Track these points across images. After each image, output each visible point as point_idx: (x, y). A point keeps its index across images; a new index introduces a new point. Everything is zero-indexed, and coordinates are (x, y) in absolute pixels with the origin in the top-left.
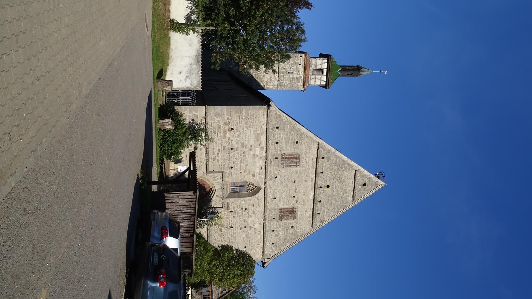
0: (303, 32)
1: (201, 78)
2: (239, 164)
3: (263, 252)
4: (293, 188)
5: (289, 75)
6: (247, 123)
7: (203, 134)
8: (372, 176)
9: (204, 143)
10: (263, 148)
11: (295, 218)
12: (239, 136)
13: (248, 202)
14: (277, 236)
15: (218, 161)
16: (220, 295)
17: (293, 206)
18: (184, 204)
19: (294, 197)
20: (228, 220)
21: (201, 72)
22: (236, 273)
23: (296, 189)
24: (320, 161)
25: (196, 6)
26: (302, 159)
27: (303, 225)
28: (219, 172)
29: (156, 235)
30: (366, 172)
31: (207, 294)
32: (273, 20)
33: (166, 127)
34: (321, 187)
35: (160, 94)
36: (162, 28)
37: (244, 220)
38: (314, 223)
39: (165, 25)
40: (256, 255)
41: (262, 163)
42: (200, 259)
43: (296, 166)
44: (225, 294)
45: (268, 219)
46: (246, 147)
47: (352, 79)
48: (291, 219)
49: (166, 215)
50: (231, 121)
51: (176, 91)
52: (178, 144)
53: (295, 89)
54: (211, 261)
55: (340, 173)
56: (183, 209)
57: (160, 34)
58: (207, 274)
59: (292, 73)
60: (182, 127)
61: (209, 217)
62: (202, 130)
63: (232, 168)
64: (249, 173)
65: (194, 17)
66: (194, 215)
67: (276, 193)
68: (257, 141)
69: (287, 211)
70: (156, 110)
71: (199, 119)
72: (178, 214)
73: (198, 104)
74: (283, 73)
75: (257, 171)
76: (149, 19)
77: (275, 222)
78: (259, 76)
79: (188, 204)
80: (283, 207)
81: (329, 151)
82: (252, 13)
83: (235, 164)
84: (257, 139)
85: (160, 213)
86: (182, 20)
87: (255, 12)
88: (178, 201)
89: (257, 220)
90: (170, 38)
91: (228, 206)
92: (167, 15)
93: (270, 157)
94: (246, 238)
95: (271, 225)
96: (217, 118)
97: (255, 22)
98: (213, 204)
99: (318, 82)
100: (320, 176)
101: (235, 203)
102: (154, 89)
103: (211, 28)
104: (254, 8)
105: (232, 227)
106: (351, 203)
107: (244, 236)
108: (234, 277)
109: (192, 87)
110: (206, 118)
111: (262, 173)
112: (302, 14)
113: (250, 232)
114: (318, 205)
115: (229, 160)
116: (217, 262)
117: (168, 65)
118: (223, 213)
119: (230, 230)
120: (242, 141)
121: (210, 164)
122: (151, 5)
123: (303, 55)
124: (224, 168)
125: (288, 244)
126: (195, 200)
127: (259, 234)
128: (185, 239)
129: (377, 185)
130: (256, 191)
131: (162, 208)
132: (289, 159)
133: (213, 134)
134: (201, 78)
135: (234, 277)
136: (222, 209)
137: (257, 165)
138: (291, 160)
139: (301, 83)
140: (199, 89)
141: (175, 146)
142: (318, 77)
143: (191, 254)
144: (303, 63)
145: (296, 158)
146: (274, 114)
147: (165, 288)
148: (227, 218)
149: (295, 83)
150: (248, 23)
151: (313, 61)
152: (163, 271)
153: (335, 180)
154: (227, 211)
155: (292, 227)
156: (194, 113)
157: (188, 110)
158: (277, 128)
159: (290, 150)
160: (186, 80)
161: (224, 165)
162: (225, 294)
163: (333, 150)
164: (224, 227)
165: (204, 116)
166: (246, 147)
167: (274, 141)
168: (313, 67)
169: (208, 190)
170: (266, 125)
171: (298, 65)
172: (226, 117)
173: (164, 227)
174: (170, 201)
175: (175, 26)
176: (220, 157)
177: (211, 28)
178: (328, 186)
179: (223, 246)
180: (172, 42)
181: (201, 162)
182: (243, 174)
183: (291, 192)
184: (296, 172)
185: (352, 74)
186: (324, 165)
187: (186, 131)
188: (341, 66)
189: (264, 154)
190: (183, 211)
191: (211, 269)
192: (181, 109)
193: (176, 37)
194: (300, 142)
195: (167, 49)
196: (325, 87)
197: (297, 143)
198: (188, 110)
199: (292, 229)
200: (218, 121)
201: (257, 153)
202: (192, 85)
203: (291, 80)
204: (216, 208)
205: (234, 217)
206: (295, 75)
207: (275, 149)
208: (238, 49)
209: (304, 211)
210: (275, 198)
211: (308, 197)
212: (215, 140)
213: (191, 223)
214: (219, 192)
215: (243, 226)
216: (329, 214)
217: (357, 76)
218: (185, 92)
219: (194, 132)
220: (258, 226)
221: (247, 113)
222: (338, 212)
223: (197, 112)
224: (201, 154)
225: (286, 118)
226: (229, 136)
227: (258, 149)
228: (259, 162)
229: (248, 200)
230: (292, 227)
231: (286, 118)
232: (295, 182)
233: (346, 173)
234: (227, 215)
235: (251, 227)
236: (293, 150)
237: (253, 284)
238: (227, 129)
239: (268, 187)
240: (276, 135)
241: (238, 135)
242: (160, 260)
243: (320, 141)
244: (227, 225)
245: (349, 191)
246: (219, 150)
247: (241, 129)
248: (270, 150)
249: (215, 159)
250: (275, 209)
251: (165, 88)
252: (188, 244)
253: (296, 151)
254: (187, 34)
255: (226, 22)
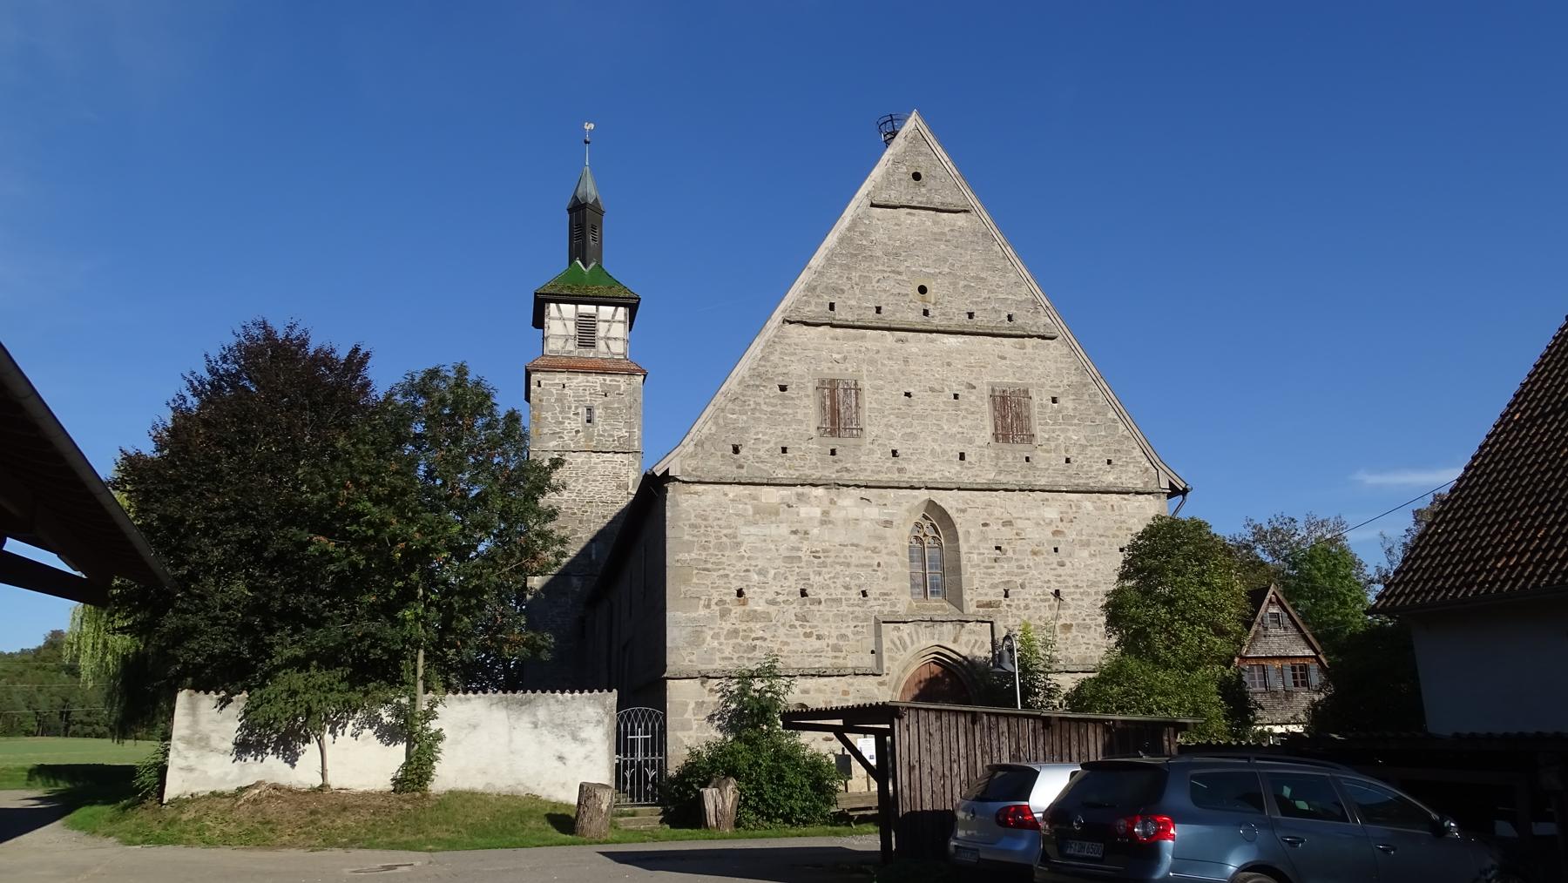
0: (433, 374)
1: (577, 694)
2: (853, 570)
3: (1138, 493)
4: (931, 403)
5: (596, 420)
6: (721, 547)
7: (757, 684)
8: (888, 155)
9: (785, 681)
10: (800, 496)
11: (1026, 392)
12: (762, 572)
13: (973, 541)
14: (1084, 447)
15: (843, 636)
16: (1292, 631)
17: (987, 398)
18: (937, 748)
19: (956, 396)
20: (1033, 605)
21: (558, 694)
22: (1195, 580)
23: (932, 390)
24: (841, 315)
25: (350, 708)
26: (836, 372)
27: (1047, 367)
28: (878, 635)
29: (1023, 845)
30: (877, 172)
31: (1289, 674)
32: (395, 467)
33: (729, 804)
34: (926, 313)
35: (627, 823)
36: (417, 819)
37: (1035, 553)
38: (1042, 332)
39: (408, 806)
40: (1144, 512)
41: (848, 501)
42: (1149, 696)
43: (858, 390)
44: (1290, 616)
45: (1031, 479)
46: (799, 549)
47: (611, 229)
48: (1027, 405)
49: (965, 810)
50: (716, 597)
51: (619, 770)
52: (783, 765)
53: (640, 400)
54: (1156, 660)
55: (879, 254)
56: (955, 753)
57: (434, 823)
58: (1199, 674)
59: (589, 410)
60: (732, 754)
61: (1009, 667)
62: (743, 692)
63: (864, 594)
64: (880, 538)
65: (386, 716)
66: (975, 717)
67: (944, 452)
68: (777, 513)
69: (1004, 417)
70: (674, 838)
71: (707, 699)
72: (972, 768)
73: (660, 701)
74: (589, 437)
75: (873, 512)
76: (376, 858)
77: (1039, 457)
78: (601, 511)
79: (937, 736)
80: (990, 430)
81: (811, 289)
82: (371, 532)
83: (853, 583)
84: (772, 512)
85: (961, 833)
86: (397, 754)
87: (370, 524)
88: (926, 770)
89: (1033, 514)
90: (451, 792)
91: (989, 605)
92: (378, 802)
93: (831, 474)
94: (1092, 548)
95: (1047, 466)
96: (703, 642)
97: (395, 525)
98: (983, 652)
99: (619, 330)
100: (888, 317)
101: (977, 585)
102: (606, 842)
103: (421, 661)
104: (355, 527)
105: (1057, 593)
106: (974, 217)
107: (1085, 554)
108: (1208, 585)
109: (607, 720)
110: (707, 677)
111: (880, 497)
112: (384, 378)
113: (1072, 535)
114: (982, 320)
115: (838, 601)
116: (1159, 641)
117: (537, 798)
118: (1011, 621)
119: (1068, 599)
120: (779, 563)
121: (851, 662)
122: (338, 852)
123: (535, 377)
124: (866, 620)
125: (1112, 414)
126: (922, 713)
127: (1079, 507)
128: (1057, 748)
129: (918, 138)
130: (938, 517)
131: (944, 821)
132: (835, 412)
133: (757, 654)
134: (577, 694)
135: (1208, 585)
136: (999, 625)
137: (854, 512)
138: (838, 410)
139: (622, 381)
140: (612, 697)
141: (790, 776)
142: (602, 329)
143: (1107, 727)
144: (560, 378)
145: (833, 391)
146: (693, 463)
147: (1180, 818)
148: (1027, 607)
150: (401, 545)
151: (553, 346)
152: (1122, 824)
153: (902, 269)
154: (1003, 607)
155: (1054, 400)
156: (688, 715)
157: (679, 734)
158: (736, 450)
159: (808, 411)
160: (583, 741)
161: (856, 618)
162: (1290, 616)
163: (805, 277)
164: (1058, 617)
165: (698, 682)
166: (799, 549)
167: (779, 460)
168: (571, 346)
169: (937, 669)
170: (726, 487)
171: (566, 391)
172: (702, 612)
173: (997, 815)
174: (927, 796)
175: (415, 775)
176: (830, 631)
177: (421, 661)
178: (923, 290)
179: (1108, 624)
180: (464, 784)
181: (845, 693)
182: (883, 559)
183: (942, 406)
184: (878, 389)
185: (594, 228)
186: (853, 302)
187: (747, 741)
188: (571, 261)
189: (820, 491)
190: (962, 751)
191: (1184, 662)
192: (677, 756)
193: (448, 775)
194: (781, 380)
195: (487, 802)
196: (633, 309)
197: (783, 388)
198: (679, 734)
199: (1061, 401)
200: (716, 636)
201: (817, 512)
202: (599, 722)
204: (993, 642)
205: (1022, 586)
207: (803, 458)
208: (480, 577)
209: (1004, 363)
210: (962, 456)
211: (958, 351)
212: (776, 646)
213: (1003, 726)
214: (941, 633)
215: (1054, 558)
216: (1011, 286)
217: (601, 213)
218: (622, 744)
219: (752, 714)
220: (1052, 509)
221: (688, 547)
222: (1005, 257)
223: (687, 705)
224: (819, 691)
225: (705, 423)
226: (762, 602)
227: (804, 511)
228: (844, 508)
229: (967, 540)
230: (1054, 400)
231: (705, 423)
232: (908, 394)
233: (879, 236)
234: (1018, 608)
235: (1055, 533)
236: (806, 401)
237: (1266, 527)
238: (740, 609)
239: (925, 478)
240: (759, 456)
241: (759, 573)
242: (1089, 833)
243: (778, 316)
244: (1051, 607)
245: (935, 223)
246: (808, 635)
247: (741, 565)
248: (808, 472)
249: (836, 648)
250: (998, 457)
251: (604, 807)
252: (1074, 735)
253: (810, 391)
254: (438, 736)
255: (400, 615)
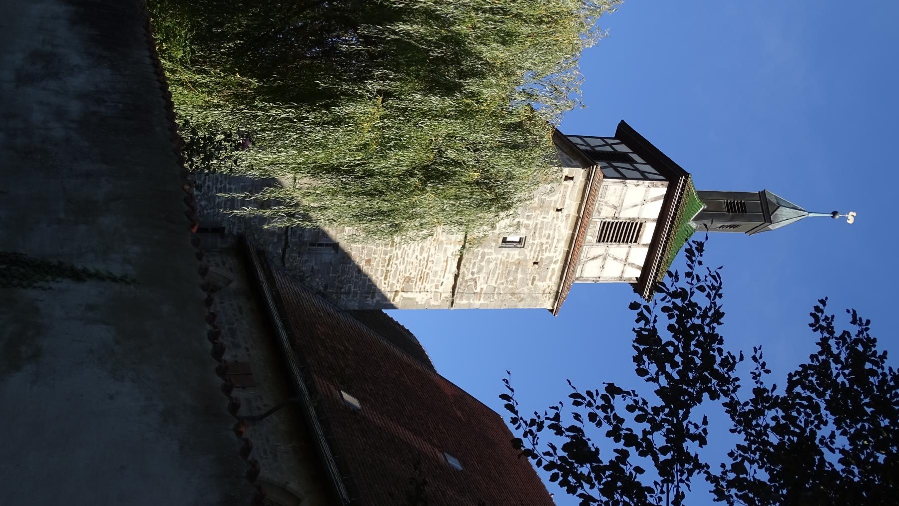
5: (505, 251)
53: (521, 306)
142: (618, 250)
144: (571, 208)
149: (524, 282)
171: (553, 213)
203: (509, 270)
206: (529, 253)
